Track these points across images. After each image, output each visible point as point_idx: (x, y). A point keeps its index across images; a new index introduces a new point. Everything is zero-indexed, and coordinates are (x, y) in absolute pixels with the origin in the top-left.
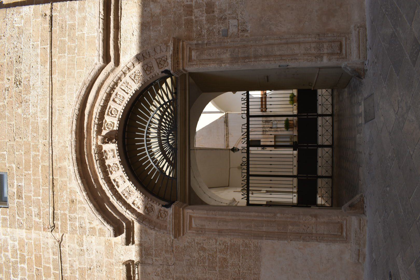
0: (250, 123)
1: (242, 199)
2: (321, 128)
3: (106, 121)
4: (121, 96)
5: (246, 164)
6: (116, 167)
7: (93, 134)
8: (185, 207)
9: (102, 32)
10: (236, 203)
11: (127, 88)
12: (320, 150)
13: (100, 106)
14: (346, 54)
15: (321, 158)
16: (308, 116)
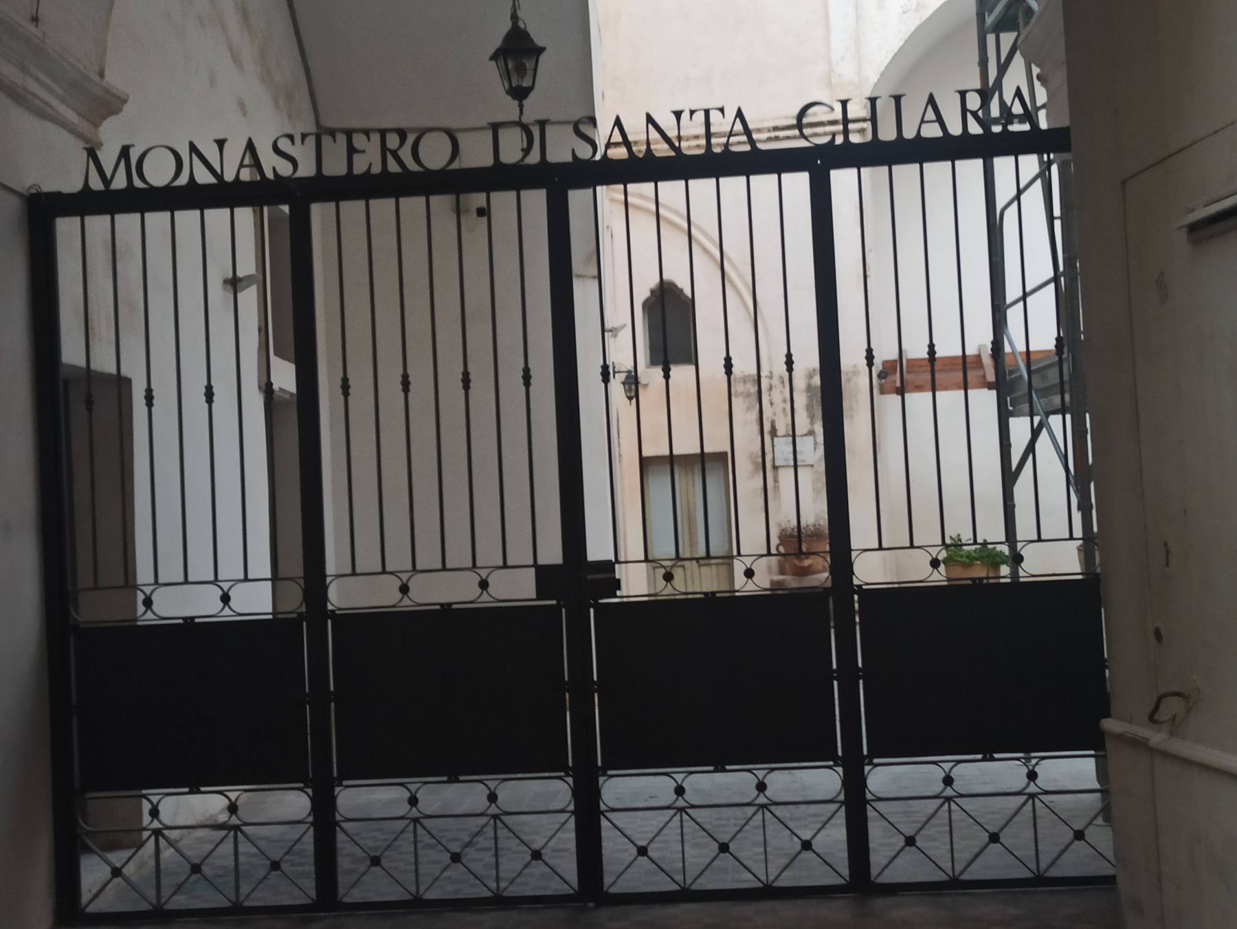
0: (764, 183)
2: (401, 813)
5: (393, 167)
15: (404, 809)
16: (848, 674)
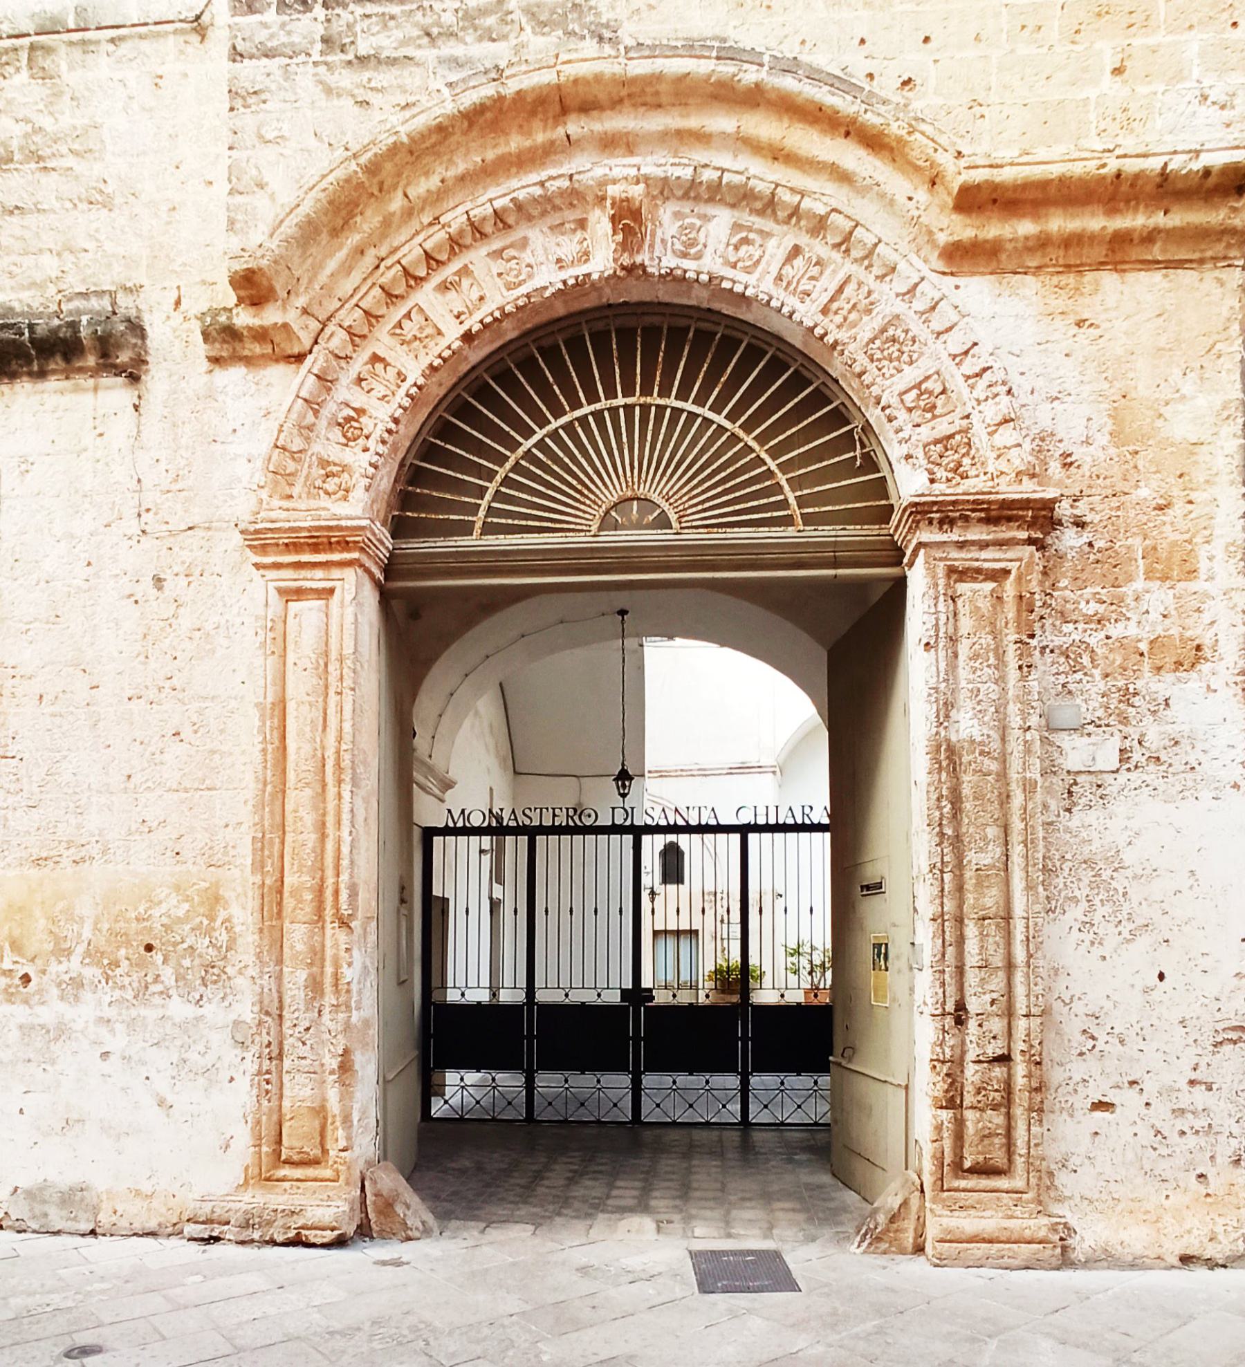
1: (449, 811)
3: (706, 218)
4: (813, 282)
6: (517, 276)
7: (655, 164)
8: (368, 571)
9: (1102, 171)
10: (437, 791)
11: (850, 306)
12: (625, 1080)
13: (773, 186)
14: (957, 1190)
